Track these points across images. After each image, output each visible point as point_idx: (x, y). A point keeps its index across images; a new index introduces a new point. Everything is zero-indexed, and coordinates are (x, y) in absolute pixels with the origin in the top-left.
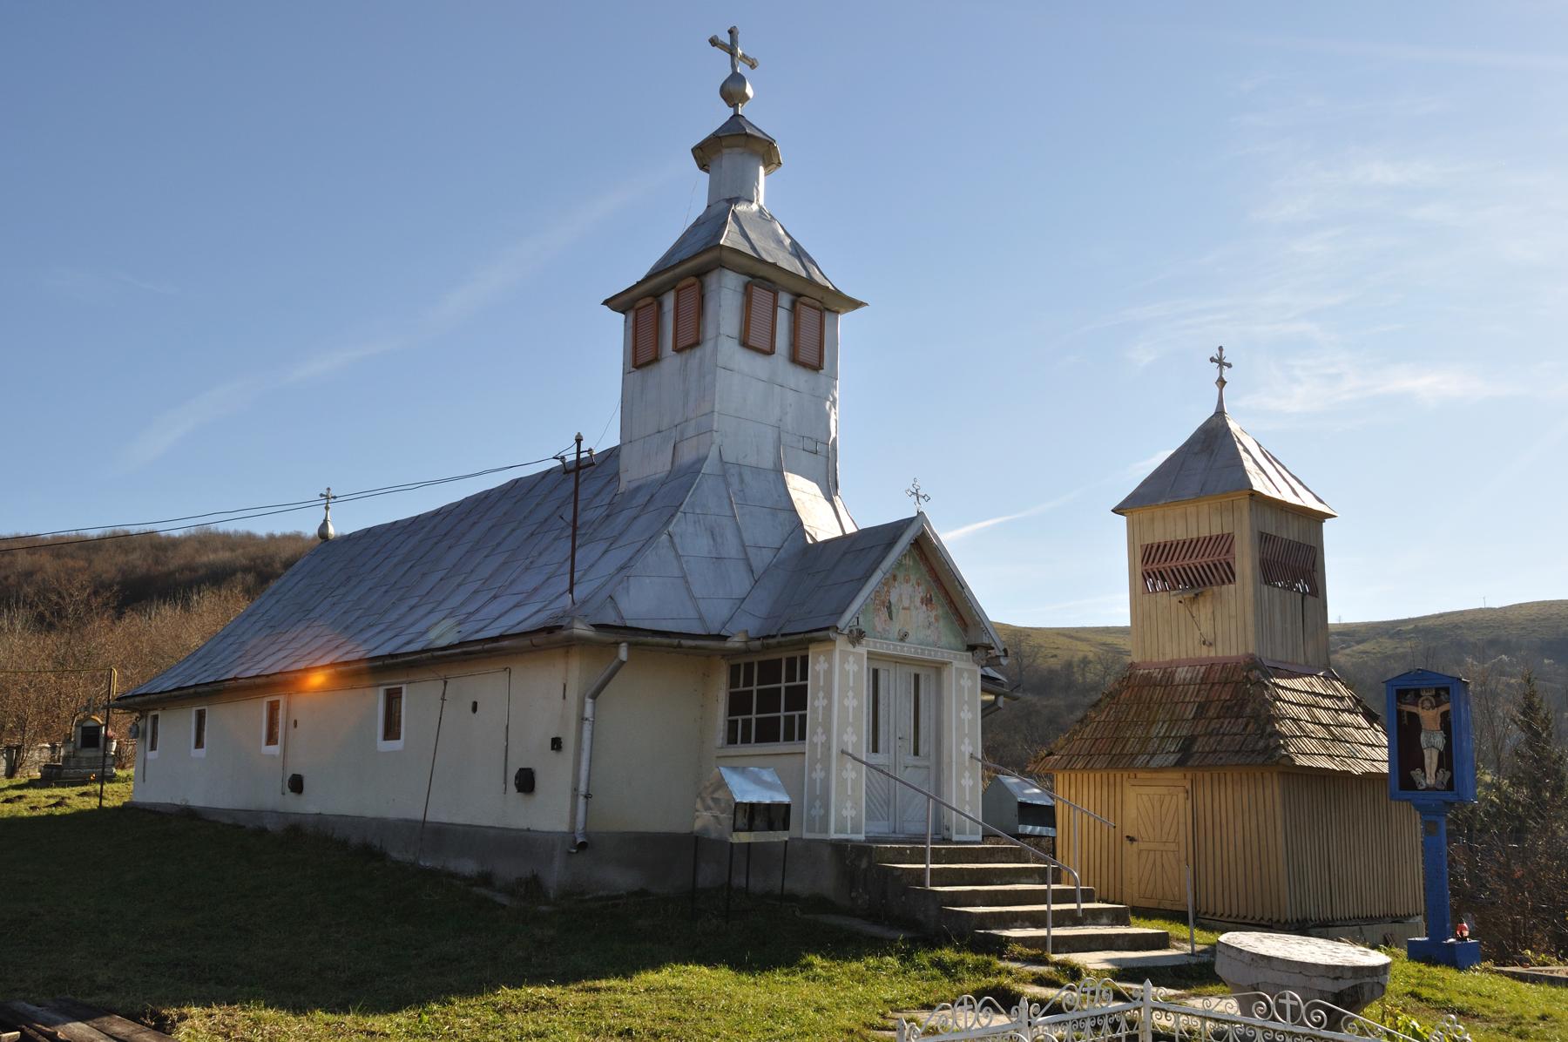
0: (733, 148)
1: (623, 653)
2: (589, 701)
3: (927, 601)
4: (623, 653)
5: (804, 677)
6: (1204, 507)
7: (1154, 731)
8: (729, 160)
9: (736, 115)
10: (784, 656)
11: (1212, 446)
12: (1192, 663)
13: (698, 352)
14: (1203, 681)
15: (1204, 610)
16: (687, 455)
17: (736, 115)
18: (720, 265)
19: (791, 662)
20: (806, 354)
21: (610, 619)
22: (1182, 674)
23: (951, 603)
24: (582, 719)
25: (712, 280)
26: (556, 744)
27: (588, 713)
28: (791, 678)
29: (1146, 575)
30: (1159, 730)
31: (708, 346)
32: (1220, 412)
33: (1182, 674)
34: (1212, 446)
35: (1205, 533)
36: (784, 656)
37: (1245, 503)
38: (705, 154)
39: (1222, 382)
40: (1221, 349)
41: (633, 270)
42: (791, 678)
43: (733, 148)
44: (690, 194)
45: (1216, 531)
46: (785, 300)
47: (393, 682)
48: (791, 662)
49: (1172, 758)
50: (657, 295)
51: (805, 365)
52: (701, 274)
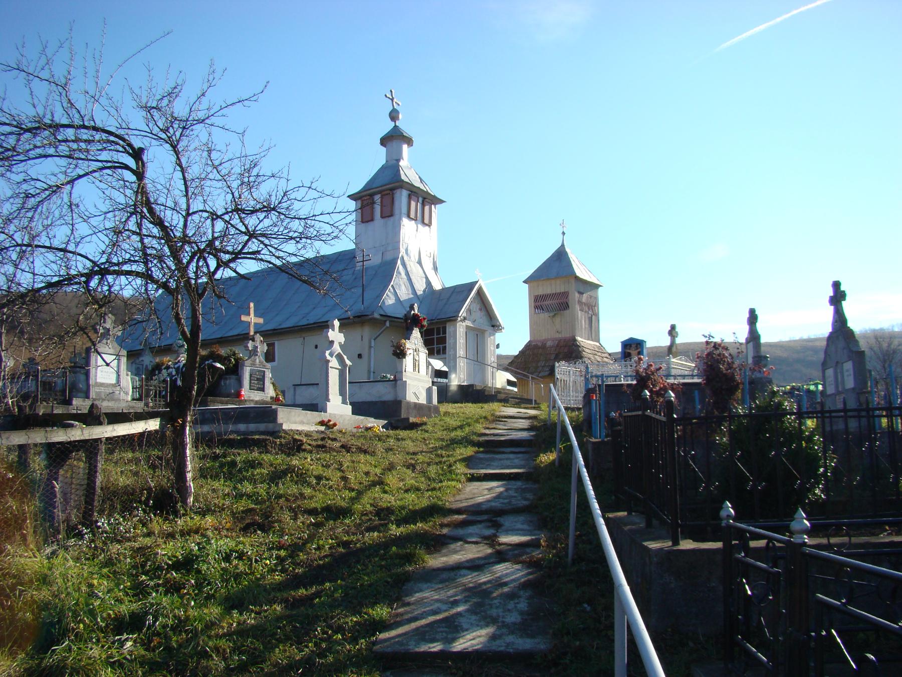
0: (394, 139)
1: (388, 324)
2: (373, 341)
3: (481, 310)
4: (388, 324)
5: (445, 332)
6: (558, 282)
7: (539, 364)
8: (395, 144)
9: (395, 126)
10: (435, 327)
11: (560, 257)
12: (553, 340)
13: (392, 218)
14: (557, 346)
15: (557, 320)
16: (389, 257)
17: (395, 126)
18: (401, 187)
19: (438, 329)
20: (426, 221)
21: (383, 313)
22: (549, 344)
23: (487, 311)
24: (370, 347)
25: (397, 193)
26: (360, 356)
27: (373, 344)
28: (438, 333)
29: (536, 307)
30: (542, 363)
31: (396, 217)
32: (563, 245)
33: (549, 344)
34: (560, 257)
35: (558, 291)
36: (435, 327)
37: (573, 281)
38: (384, 141)
39: (564, 233)
40: (753, 318)
41: (357, 186)
42: (438, 333)
43: (394, 139)
44: (379, 157)
45: (562, 290)
46: (421, 199)
47: (271, 341)
48: (438, 329)
49: (547, 373)
50: (372, 195)
51: (427, 225)
52: (392, 190)
